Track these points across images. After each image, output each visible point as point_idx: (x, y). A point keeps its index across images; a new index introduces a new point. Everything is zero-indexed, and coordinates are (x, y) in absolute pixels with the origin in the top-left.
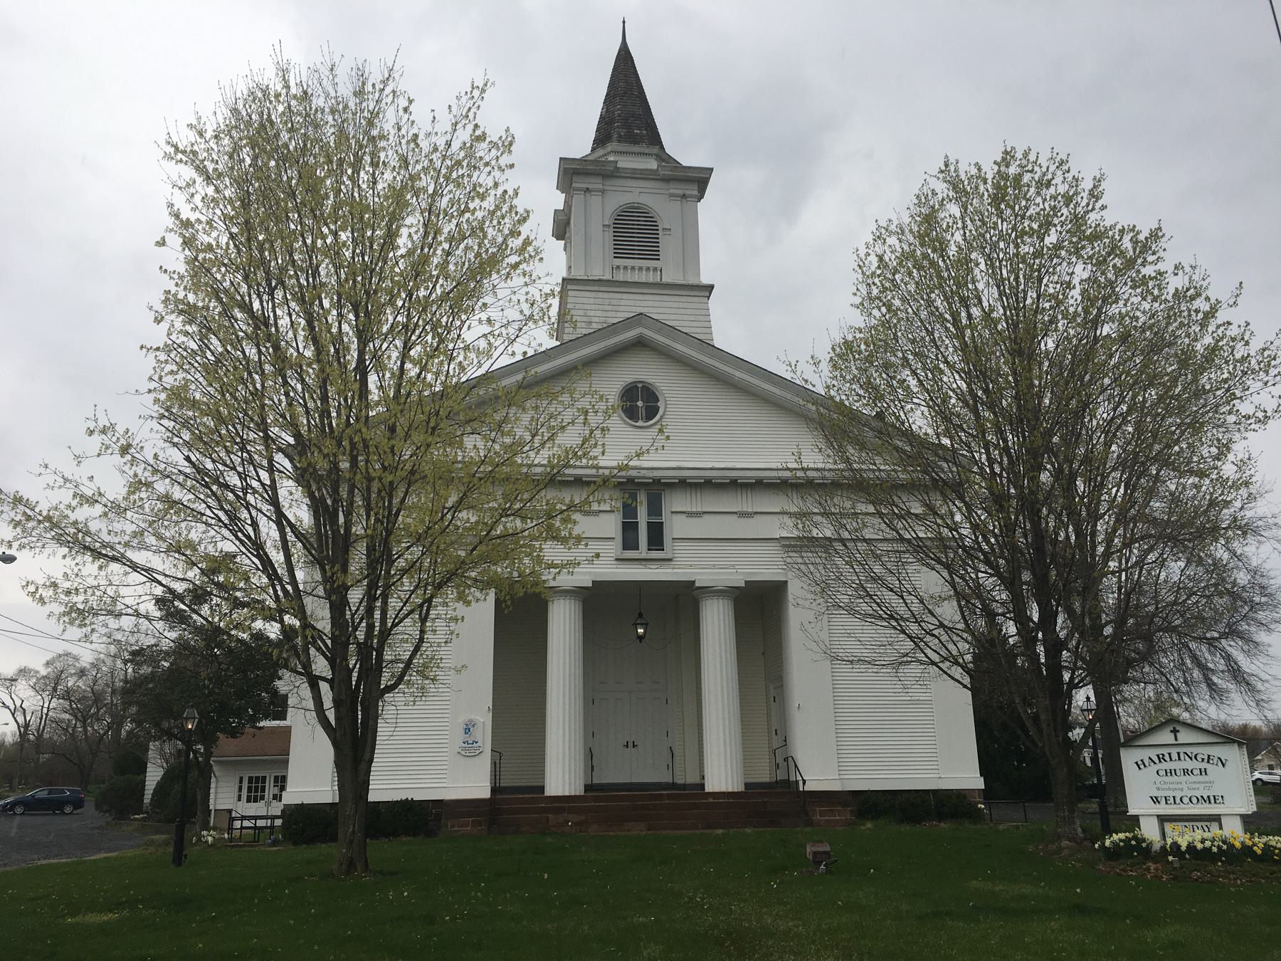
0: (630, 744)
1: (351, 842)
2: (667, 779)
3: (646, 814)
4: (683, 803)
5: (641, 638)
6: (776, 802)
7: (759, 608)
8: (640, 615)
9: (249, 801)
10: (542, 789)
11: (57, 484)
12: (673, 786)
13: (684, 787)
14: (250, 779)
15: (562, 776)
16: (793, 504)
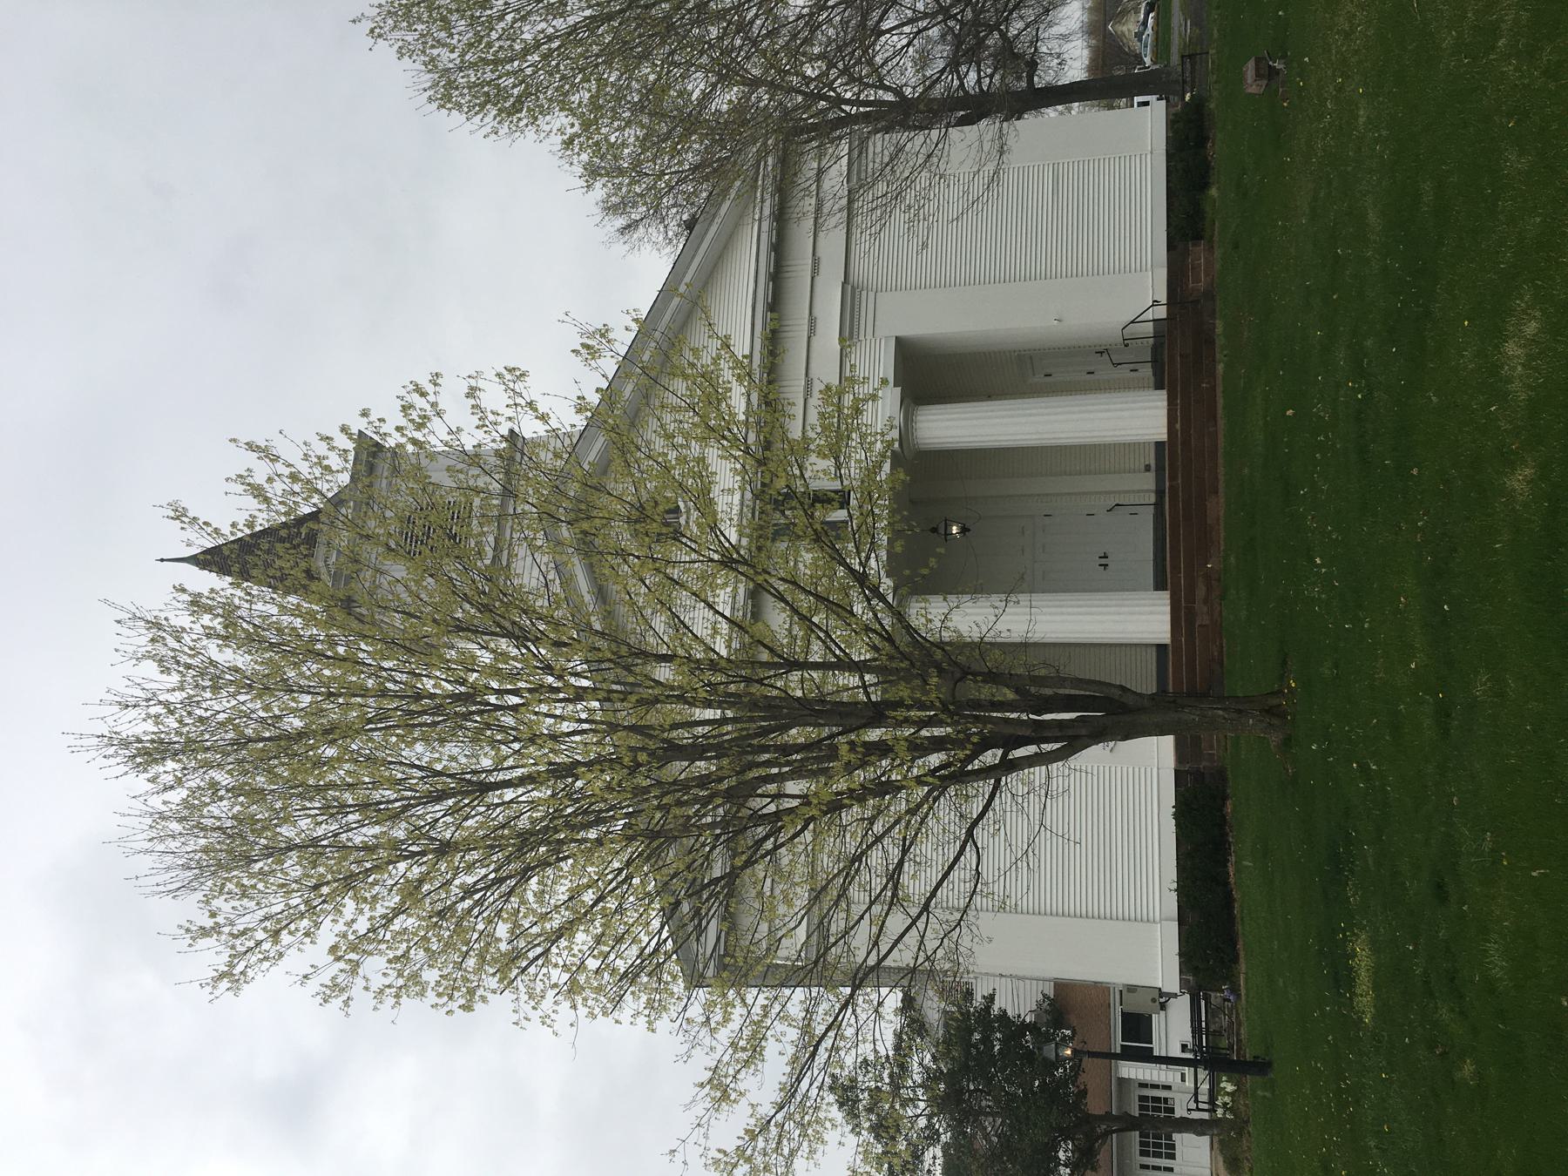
0: (1103, 561)
1: (1240, 711)
2: (1148, 516)
3: (1193, 517)
4: (1180, 462)
5: (964, 530)
6: (1180, 351)
7: (928, 374)
8: (934, 530)
9: (1172, 1157)
10: (1161, 648)
11: (702, 1141)
12: (1158, 505)
13: (1160, 492)
14: (1143, 1153)
15: (1146, 619)
16: (802, 232)
